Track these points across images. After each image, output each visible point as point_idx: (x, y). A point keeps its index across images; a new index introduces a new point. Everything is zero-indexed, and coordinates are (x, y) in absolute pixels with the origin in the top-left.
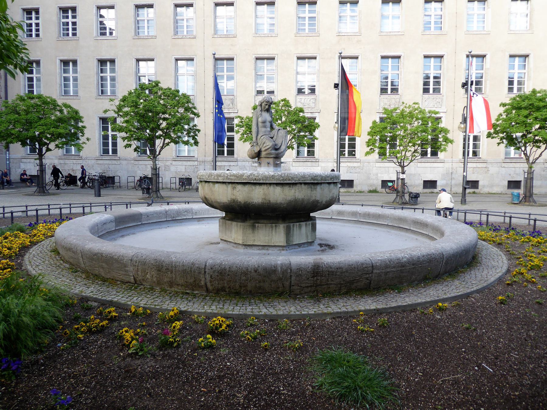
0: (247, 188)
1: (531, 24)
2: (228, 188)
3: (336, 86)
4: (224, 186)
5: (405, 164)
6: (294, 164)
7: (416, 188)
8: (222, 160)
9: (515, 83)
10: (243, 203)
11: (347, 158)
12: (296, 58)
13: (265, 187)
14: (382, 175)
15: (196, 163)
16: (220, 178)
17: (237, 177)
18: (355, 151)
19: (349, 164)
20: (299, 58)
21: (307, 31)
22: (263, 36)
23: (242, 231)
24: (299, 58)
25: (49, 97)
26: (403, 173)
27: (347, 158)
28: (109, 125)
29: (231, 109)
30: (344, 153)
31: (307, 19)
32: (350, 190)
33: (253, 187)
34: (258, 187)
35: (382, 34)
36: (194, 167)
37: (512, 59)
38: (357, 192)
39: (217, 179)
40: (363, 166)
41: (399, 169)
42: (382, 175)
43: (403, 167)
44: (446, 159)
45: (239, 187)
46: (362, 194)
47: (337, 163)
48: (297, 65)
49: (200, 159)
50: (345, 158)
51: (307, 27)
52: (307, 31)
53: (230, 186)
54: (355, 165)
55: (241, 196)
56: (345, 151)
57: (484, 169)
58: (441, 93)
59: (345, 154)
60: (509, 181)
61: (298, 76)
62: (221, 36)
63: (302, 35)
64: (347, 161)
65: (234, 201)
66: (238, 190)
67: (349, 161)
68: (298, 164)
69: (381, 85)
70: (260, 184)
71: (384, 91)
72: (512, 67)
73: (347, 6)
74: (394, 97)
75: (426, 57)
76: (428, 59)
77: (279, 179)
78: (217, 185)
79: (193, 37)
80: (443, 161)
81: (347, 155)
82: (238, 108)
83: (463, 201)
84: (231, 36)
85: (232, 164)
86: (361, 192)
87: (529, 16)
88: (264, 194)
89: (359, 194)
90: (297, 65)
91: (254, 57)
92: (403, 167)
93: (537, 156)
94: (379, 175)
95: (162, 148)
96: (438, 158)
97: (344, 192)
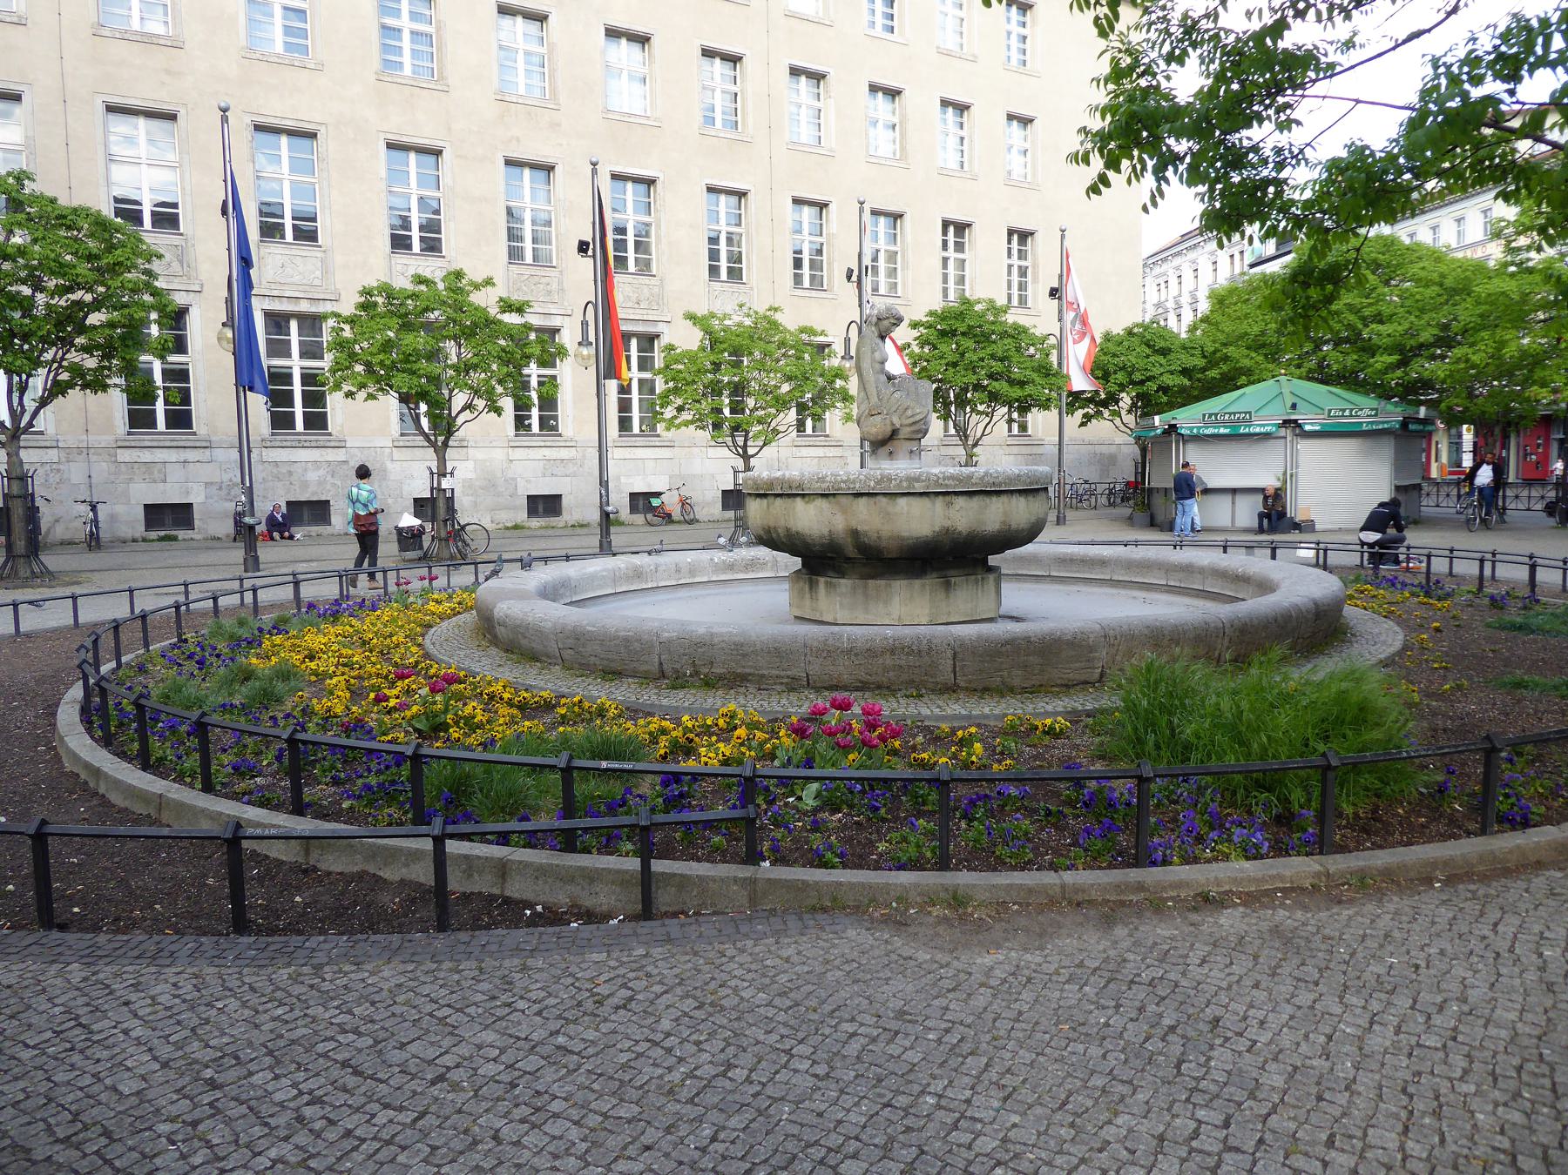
0: (976, 502)
1: (903, 149)
2: (934, 504)
3: (583, 247)
4: (925, 501)
5: (751, 451)
6: (397, 454)
7: (706, 509)
8: (155, 444)
9: (806, 264)
10: (965, 533)
11: (538, 435)
12: (101, 108)
13: (1004, 498)
14: (631, 480)
15: (53, 455)
16: (916, 485)
17: (960, 481)
18: (555, 418)
19: (546, 452)
20: (111, 109)
21: (408, 70)
22: (276, 60)
23: (928, 597)
24: (111, 109)
25: (1137, 325)
26: (748, 468)
27: (538, 435)
28: (656, 354)
29: (176, 280)
30: (527, 422)
31: (406, 36)
32: (553, 521)
33: (987, 500)
34: (994, 499)
35: (610, 116)
36: (47, 467)
37: (713, 196)
38: (573, 526)
39: (909, 487)
40: (584, 456)
41: (740, 463)
42: (631, 480)
43: (746, 457)
44: (213, 438)
45: (960, 502)
46: (585, 531)
47: (241, 452)
48: (105, 125)
49: (70, 441)
50: (534, 435)
51: (407, 59)
52: (408, 70)
53: (940, 501)
54: (564, 454)
55: (964, 520)
56: (529, 417)
57: (838, 460)
58: (1029, 305)
59: (530, 425)
60: (416, 500)
61: (114, 167)
62: (126, 36)
63: (399, 80)
64: (542, 444)
65: (947, 531)
66: (957, 507)
67: (548, 444)
68: (407, 453)
69: (261, 211)
70: (998, 493)
71: (400, 243)
72: (714, 216)
73: (619, 44)
74: (647, 282)
75: (711, 190)
76: (620, 184)
77: (1025, 483)
78: (902, 501)
79: (15, 20)
80: (204, 444)
81: (535, 428)
82: (203, 276)
83: (250, 561)
84: (161, 42)
85: (191, 455)
86: (582, 526)
87: (897, 128)
88: (1005, 513)
89: (579, 531)
90: (106, 132)
91: (248, 120)
92: (746, 457)
93: (979, 434)
94: (623, 480)
95: (43, 403)
96: (330, 434)
97: (541, 528)
